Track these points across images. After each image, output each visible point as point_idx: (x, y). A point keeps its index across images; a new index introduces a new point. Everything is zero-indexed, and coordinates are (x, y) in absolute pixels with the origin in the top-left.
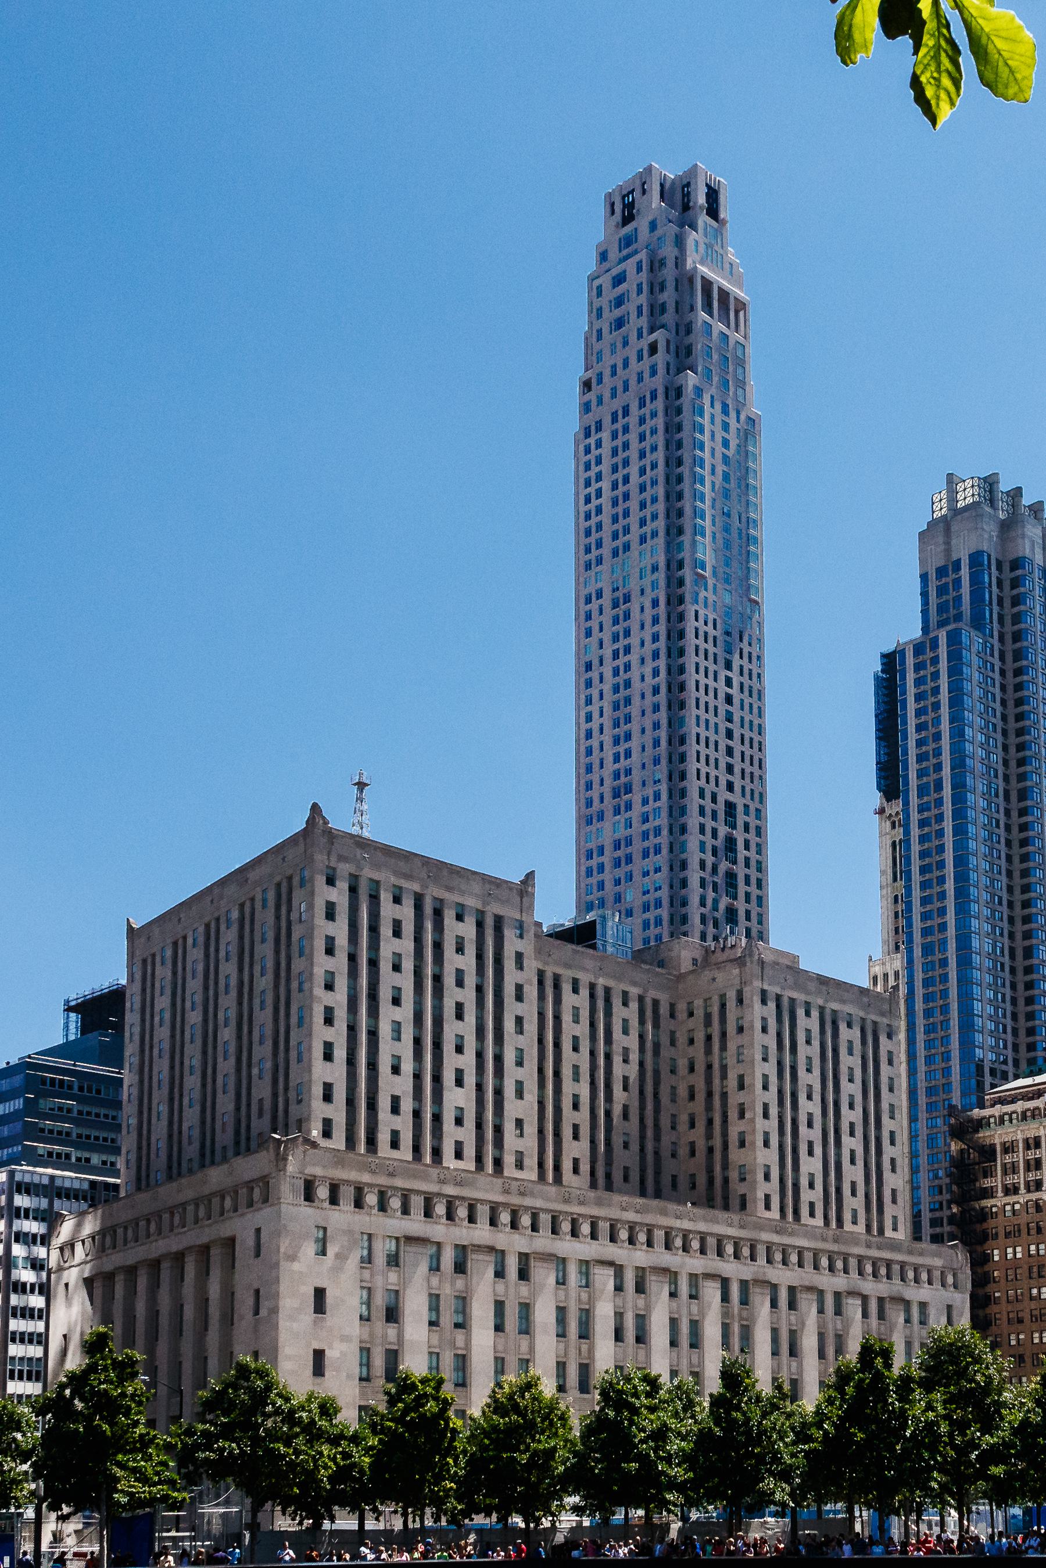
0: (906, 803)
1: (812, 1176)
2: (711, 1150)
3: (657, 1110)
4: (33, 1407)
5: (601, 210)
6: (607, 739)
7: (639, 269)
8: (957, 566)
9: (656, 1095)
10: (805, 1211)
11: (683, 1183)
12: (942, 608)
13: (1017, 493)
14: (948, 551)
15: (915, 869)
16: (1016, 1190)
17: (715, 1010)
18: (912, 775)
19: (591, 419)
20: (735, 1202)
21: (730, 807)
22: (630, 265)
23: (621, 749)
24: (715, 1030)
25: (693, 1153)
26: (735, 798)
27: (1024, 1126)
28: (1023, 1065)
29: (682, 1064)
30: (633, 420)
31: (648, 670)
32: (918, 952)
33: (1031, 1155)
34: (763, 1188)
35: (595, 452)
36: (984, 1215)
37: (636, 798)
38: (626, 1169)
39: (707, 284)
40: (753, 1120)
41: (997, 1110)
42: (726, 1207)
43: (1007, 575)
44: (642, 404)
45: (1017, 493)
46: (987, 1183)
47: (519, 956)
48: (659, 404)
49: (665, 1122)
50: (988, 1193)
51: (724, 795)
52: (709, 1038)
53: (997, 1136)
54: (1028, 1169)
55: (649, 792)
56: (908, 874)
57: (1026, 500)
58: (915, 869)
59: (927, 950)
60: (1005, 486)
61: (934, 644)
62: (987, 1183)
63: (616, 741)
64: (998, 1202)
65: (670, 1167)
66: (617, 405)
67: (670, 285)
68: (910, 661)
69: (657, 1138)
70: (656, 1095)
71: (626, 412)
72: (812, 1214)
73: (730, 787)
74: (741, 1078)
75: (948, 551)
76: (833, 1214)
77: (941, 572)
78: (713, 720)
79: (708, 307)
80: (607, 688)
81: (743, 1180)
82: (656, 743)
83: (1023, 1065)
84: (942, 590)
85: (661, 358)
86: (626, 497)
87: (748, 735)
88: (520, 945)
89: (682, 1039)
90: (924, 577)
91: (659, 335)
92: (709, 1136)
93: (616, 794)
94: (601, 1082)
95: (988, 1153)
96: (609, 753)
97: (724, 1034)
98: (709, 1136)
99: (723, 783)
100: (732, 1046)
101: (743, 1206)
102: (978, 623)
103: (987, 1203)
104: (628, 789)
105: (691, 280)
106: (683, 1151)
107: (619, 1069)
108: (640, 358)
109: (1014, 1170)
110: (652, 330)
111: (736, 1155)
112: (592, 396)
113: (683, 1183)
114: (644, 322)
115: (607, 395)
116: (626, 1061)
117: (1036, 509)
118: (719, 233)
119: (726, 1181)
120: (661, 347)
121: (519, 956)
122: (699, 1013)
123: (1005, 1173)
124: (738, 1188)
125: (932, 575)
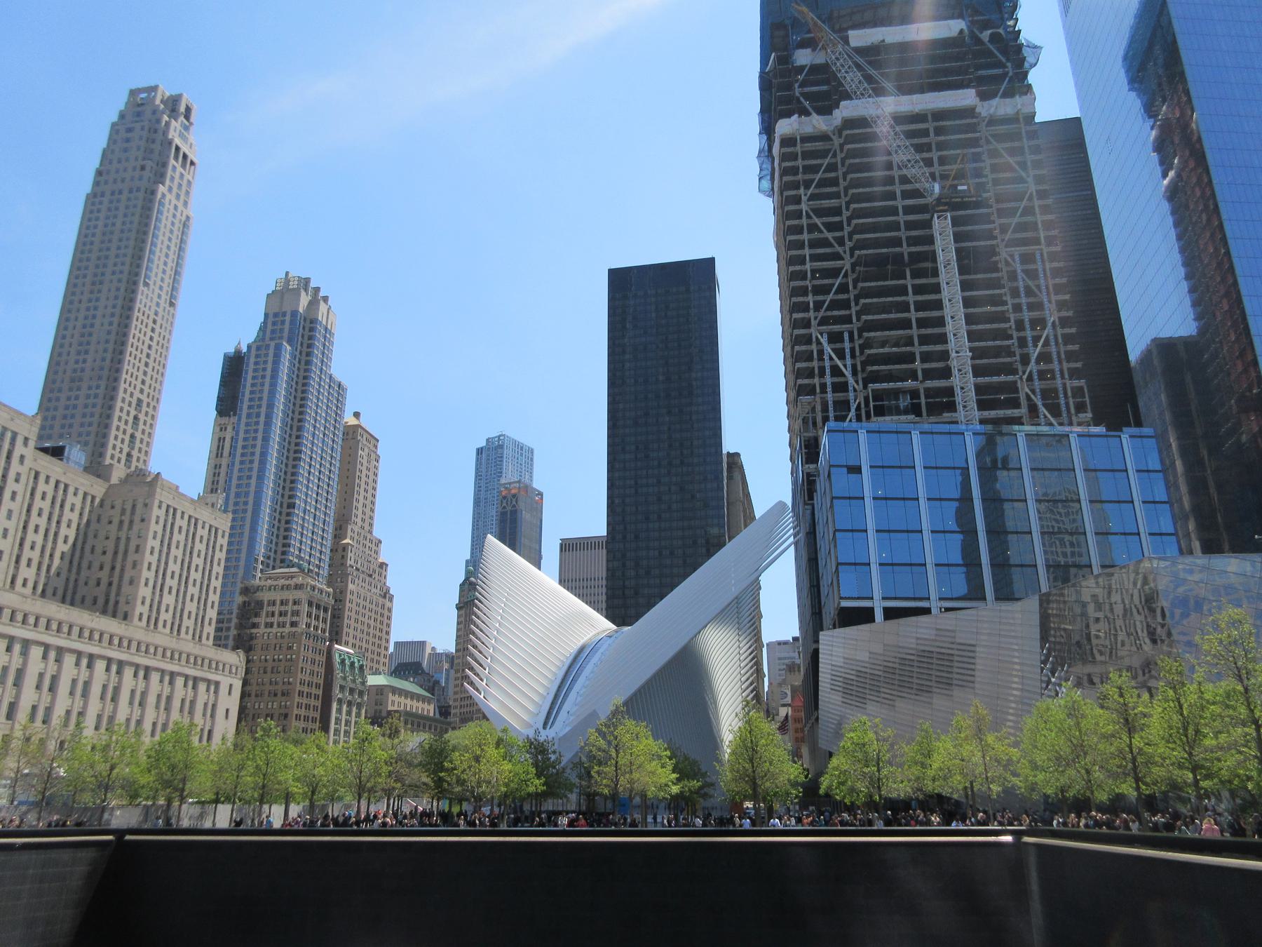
0: (239, 420)
1: (168, 606)
2: (110, 584)
3: (81, 558)
5: (127, 93)
6: (73, 351)
7: (142, 129)
8: (284, 314)
9: (83, 548)
10: (160, 624)
11: (89, 600)
12: (273, 332)
13: (317, 290)
16: (272, 626)
17: (128, 507)
18: (245, 407)
20: (120, 614)
21: (140, 401)
22: (138, 126)
24: (126, 519)
25: (98, 584)
26: (144, 397)
28: (278, 562)
30: (105, 200)
31: (106, 321)
32: (232, 495)
33: (296, 608)
34: (139, 609)
36: (252, 638)
37: (85, 385)
38: (56, 588)
39: (177, 148)
40: (140, 571)
42: (114, 616)
45: (317, 290)
46: (256, 620)
47: (22, 457)
48: (141, 195)
49: (85, 564)
50: (255, 626)
51: (137, 394)
52: (121, 522)
53: (265, 596)
54: (281, 615)
55: (94, 384)
56: (234, 456)
57: (322, 294)
59: (238, 495)
60: (313, 284)
61: (268, 346)
62: (256, 620)
63: (79, 353)
64: (262, 630)
65: (82, 590)
67: (158, 142)
69: (78, 573)
70: (83, 548)
72: (164, 626)
74: (138, 546)
76: (176, 628)
77: (276, 315)
78: (139, 355)
79: (176, 158)
80: (79, 324)
81: (127, 603)
82: (103, 360)
83: (278, 562)
84: (274, 324)
85: (147, 174)
87: (157, 367)
88: (24, 451)
89: (104, 520)
90: (266, 315)
91: (149, 164)
92: (111, 575)
93: (72, 380)
94: (51, 535)
95: (260, 604)
96: (73, 357)
97: (131, 522)
98: (111, 575)
99: (138, 388)
100: (136, 527)
101: (125, 617)
102: (290, 341)
103: (254, 631)
106: (92, 583)
107: (64, 531)
109: (273, 615)
110: (144, 159)
111: (126, 589)
112: (102, 179)
113: (89, 600)
116: (69, 526)
117: (326, 299)
118: (187, 128)
119: (117, 602)
120: (148, 168)
121: (22, 457)
124: (122, 607)
125: (271, 316)
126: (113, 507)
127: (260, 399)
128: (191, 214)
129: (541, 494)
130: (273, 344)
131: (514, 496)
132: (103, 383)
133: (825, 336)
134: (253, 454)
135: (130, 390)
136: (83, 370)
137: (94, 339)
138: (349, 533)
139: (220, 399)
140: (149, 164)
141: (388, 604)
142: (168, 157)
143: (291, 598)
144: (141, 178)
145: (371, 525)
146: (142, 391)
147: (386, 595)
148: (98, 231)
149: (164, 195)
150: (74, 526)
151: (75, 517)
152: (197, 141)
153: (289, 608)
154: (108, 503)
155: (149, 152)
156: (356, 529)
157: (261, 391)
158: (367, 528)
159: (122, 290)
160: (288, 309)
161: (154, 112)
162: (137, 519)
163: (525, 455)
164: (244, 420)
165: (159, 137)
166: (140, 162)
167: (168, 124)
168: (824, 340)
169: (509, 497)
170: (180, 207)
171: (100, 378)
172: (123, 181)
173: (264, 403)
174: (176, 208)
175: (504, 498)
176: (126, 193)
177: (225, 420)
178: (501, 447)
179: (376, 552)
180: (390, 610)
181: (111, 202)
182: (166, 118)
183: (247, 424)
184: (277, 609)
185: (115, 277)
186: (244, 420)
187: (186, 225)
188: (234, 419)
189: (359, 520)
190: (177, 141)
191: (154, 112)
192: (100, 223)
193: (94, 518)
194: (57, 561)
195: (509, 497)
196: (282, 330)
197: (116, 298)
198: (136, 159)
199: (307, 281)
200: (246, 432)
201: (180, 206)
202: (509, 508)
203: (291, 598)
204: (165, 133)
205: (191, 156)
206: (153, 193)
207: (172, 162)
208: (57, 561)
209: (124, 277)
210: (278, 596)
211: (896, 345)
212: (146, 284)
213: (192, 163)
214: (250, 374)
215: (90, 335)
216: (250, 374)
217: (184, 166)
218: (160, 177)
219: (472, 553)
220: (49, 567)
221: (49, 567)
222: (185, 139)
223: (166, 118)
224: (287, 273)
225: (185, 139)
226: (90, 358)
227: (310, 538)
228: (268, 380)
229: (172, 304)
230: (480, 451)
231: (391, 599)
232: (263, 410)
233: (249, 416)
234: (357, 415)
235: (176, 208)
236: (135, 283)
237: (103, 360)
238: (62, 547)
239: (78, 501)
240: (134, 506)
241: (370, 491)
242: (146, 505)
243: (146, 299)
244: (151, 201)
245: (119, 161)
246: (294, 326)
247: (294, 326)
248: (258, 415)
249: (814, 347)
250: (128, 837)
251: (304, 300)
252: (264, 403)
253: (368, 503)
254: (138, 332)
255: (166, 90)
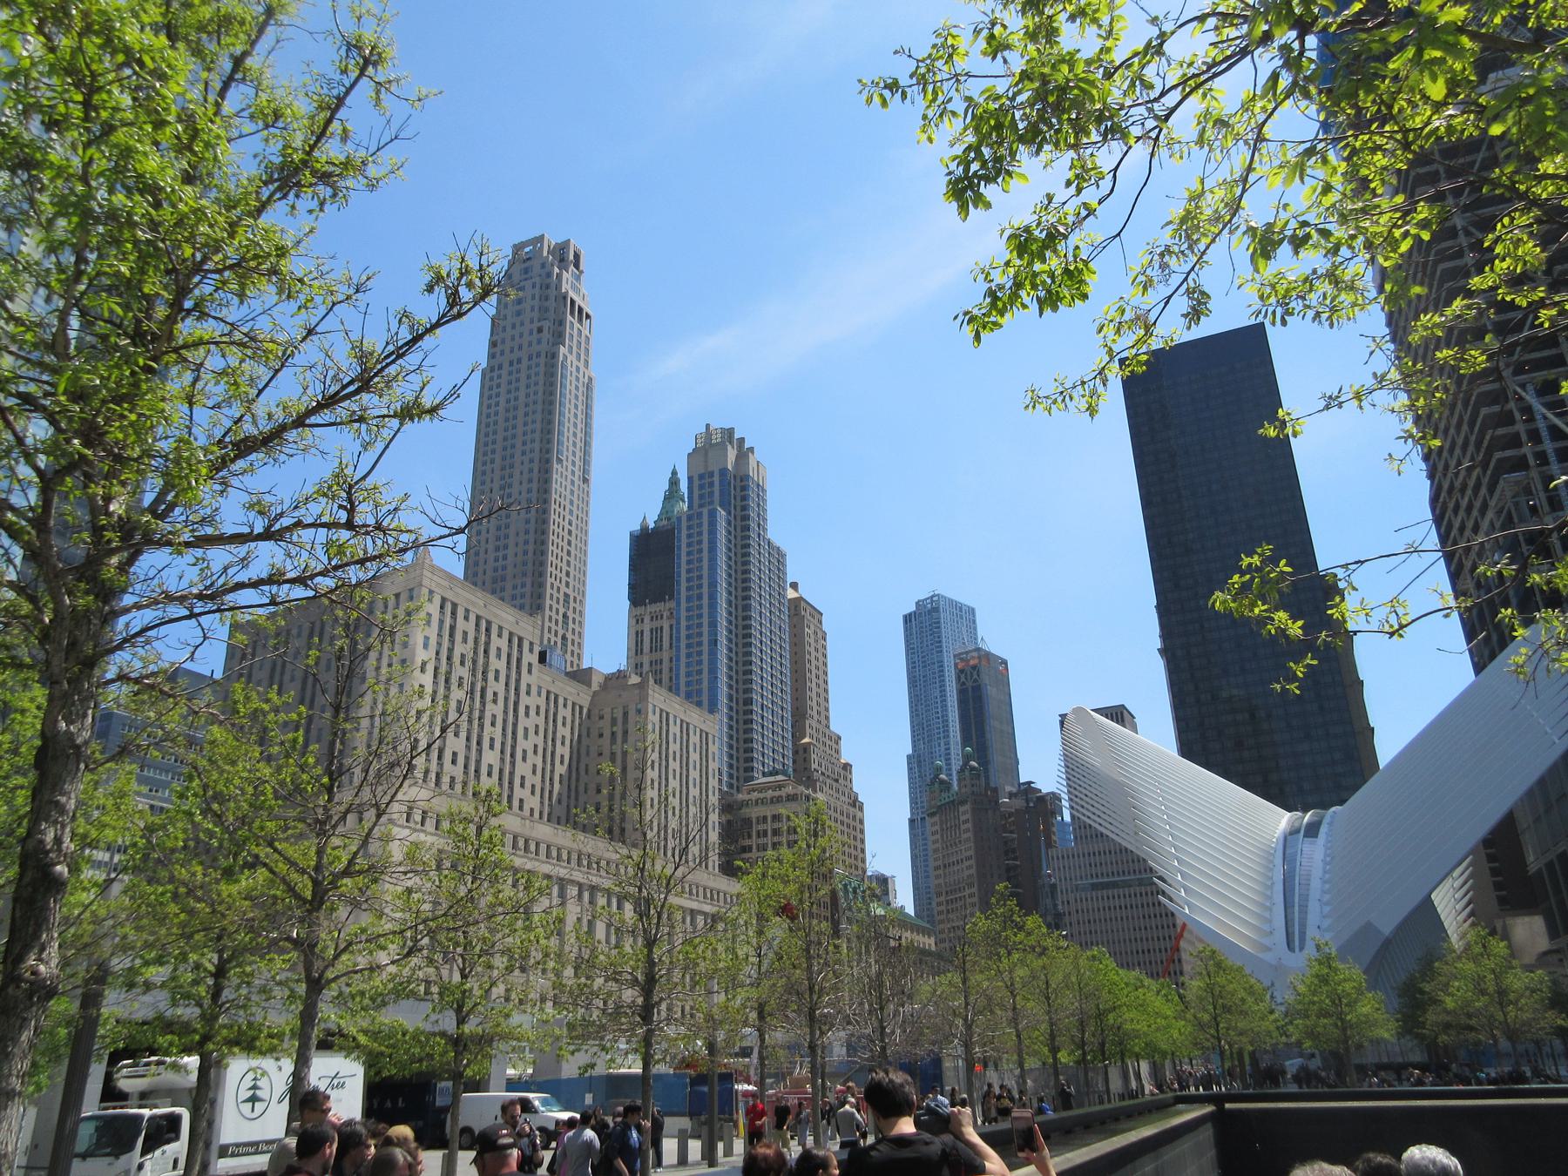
0: (679, 604)
4: (1554, 982)
8: (711, 474)
12: (701, 497)
13: (742, 440)
14: (706, 466)
15: (683, 646)
17: (619, 715)
18: (683, 589)
19: (495, 362)
22: (528, 284)
23: (500, 554)
24: (619, 729)
26: (569, 592)
27: (772, 807)
29: (593, 750)
30: (504, 372)
35: (496, 381)
39: (573, 302)
41: (755, 795)
43: (739, 484)
44: (530, 358)
45: (742, 440)
48: (542, 360)
49: (581, 788)
51: (563, 589)
53: (754, 813)
55: (519, 582)
58: (683, 646)
60: (737, 436)
61: (700, 515)
62: (747, 842)
66: (514, 356)
68: (684, 524)
71: (519, 361)
73: (567, 584)
75: (706, 466)
77: (701, 477)
79: (572, 313)
82: (525, 553)
84: (701, 487)
85: (546, 335)
86: (516, 408)
89: (595, 733)
91: (546, 324)
95: (747, 822)
96: (491, 555)
97: (625, 732)
104: (503, 579)
105: (565, 298)
108: (531, 333)
109: (765, 833)
114: (536, 314)
115: (507, 351)
118: (578, 278)
120: (545, 330)
122: (608, 717)
123: (758, 836)
125: (696, 479)
126: (601, 717)
127: (700, 577)
128: (593, 375)
129: (1005, 662)
130: (705, 511)
131: (974, 667)
132: (528, 581)
133: (1530, 387)
134: (700, 644)
135: (557, 584)
136: (504, 568)
137: (512, 532)
138: (808, 731)
139: (632, 587)
140: (546, 324)
141: (859, 814)
142: (564, 313)
143: (769, 814)
144: (539, 342)
145: (827, 718)
146: (567, 584)
147: (855, 803)
148: (501, 409)
149: (565, 357)
150: (568, 742)
151: (566, 732)
152: (586, 289)
153: (769, 827)
154: (595, 712)
155: (544, 310)
156: (814, 724)
157: (700, 568)
158: (824, 722)
159: (536, 470)
160: (715, 468)
161: (543, 266)
162: (631, 728)
163: (966, 615)
164: (684, 605)
165: (552, 293)
166: (536, 324)
167: (559, 276)
168: (1531, 398)
169: (968, 670)
170: (582, 369)
171: (524, 574)
172: (520, 348)
173: (705, 582)
174: (578, 369)
175: (962, 671)
176: (525, 362)
177: (640, 610)
178: (936, 610)
179: (837, 752)
180: (861, 822)
181: (510, 373)
182: (556, 270)
183: (688, 610)
184: (769, 827)
185: (526, 459)
186: (684, 605)
187: (589, 387)
188: (672, 604)
189: (816, 717)
190: (571, 294)
191: (543, 266)
192: (502, 400)
193: (584, 733)
194: (557, 786)
195: (968, 670)
196: (711, 494)
197: (530, 481)
198: (532, 322)
199: (731, 432)
200: (688, 618)
201: (581, 365)
202: (970, 684)
203: (769, 814)
204: (558, 286)
205: (586, 309)
206: (554, 356)
207: (569, 317)
208: (557, 786)
209: (536, 456)
210: (768, 811)
211: (1466, 409)
212: (560, 461)
213: (588, 316)
214: (684, 549)
215: (507, 526)
216: (684, 549)
217: (580, 320)
218: (559, 337)
219: (914, 746)
220: (551, 792)
221: (551, 792)
222: (578, 291)
223: (556, 270)
224: (708, 426)
225: (578, 291)
226: (510, 552)
227: (771, 744)
228: (705, 554)
229: (586, 481)
230: (908, 619)
231: (861, 809)
232: (705, 590)
233: (689, 599)
234: (794, 586)
235: (578, 369)
236: (548, 461)
237: (525, 553)
238: (561, 769)
239: (567, 713)
240: (625, 714)
241: (822, 676)
242: (639, 711)
243: (562, 479)
244: (554, 366)
245: (514, 327)
246: (721, 486)
247: (721, 486)
248: (700, 597)
249: (1512, 405)
250: (1227, 1106)
251: (732, 454)
252: (705, 582)
253: (821, 691)
254: (558, 520)
255: (553, 239)
